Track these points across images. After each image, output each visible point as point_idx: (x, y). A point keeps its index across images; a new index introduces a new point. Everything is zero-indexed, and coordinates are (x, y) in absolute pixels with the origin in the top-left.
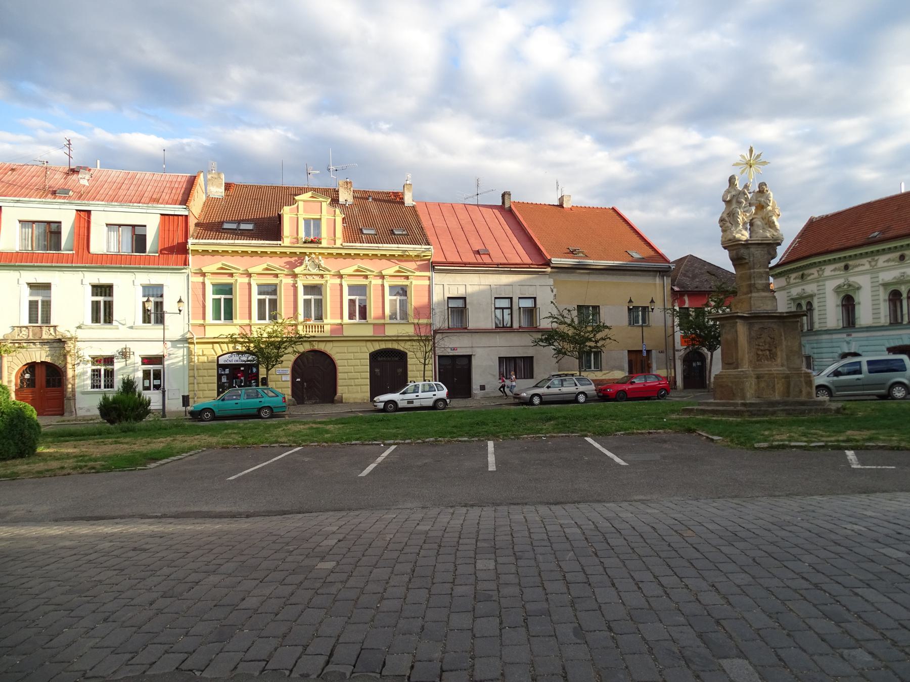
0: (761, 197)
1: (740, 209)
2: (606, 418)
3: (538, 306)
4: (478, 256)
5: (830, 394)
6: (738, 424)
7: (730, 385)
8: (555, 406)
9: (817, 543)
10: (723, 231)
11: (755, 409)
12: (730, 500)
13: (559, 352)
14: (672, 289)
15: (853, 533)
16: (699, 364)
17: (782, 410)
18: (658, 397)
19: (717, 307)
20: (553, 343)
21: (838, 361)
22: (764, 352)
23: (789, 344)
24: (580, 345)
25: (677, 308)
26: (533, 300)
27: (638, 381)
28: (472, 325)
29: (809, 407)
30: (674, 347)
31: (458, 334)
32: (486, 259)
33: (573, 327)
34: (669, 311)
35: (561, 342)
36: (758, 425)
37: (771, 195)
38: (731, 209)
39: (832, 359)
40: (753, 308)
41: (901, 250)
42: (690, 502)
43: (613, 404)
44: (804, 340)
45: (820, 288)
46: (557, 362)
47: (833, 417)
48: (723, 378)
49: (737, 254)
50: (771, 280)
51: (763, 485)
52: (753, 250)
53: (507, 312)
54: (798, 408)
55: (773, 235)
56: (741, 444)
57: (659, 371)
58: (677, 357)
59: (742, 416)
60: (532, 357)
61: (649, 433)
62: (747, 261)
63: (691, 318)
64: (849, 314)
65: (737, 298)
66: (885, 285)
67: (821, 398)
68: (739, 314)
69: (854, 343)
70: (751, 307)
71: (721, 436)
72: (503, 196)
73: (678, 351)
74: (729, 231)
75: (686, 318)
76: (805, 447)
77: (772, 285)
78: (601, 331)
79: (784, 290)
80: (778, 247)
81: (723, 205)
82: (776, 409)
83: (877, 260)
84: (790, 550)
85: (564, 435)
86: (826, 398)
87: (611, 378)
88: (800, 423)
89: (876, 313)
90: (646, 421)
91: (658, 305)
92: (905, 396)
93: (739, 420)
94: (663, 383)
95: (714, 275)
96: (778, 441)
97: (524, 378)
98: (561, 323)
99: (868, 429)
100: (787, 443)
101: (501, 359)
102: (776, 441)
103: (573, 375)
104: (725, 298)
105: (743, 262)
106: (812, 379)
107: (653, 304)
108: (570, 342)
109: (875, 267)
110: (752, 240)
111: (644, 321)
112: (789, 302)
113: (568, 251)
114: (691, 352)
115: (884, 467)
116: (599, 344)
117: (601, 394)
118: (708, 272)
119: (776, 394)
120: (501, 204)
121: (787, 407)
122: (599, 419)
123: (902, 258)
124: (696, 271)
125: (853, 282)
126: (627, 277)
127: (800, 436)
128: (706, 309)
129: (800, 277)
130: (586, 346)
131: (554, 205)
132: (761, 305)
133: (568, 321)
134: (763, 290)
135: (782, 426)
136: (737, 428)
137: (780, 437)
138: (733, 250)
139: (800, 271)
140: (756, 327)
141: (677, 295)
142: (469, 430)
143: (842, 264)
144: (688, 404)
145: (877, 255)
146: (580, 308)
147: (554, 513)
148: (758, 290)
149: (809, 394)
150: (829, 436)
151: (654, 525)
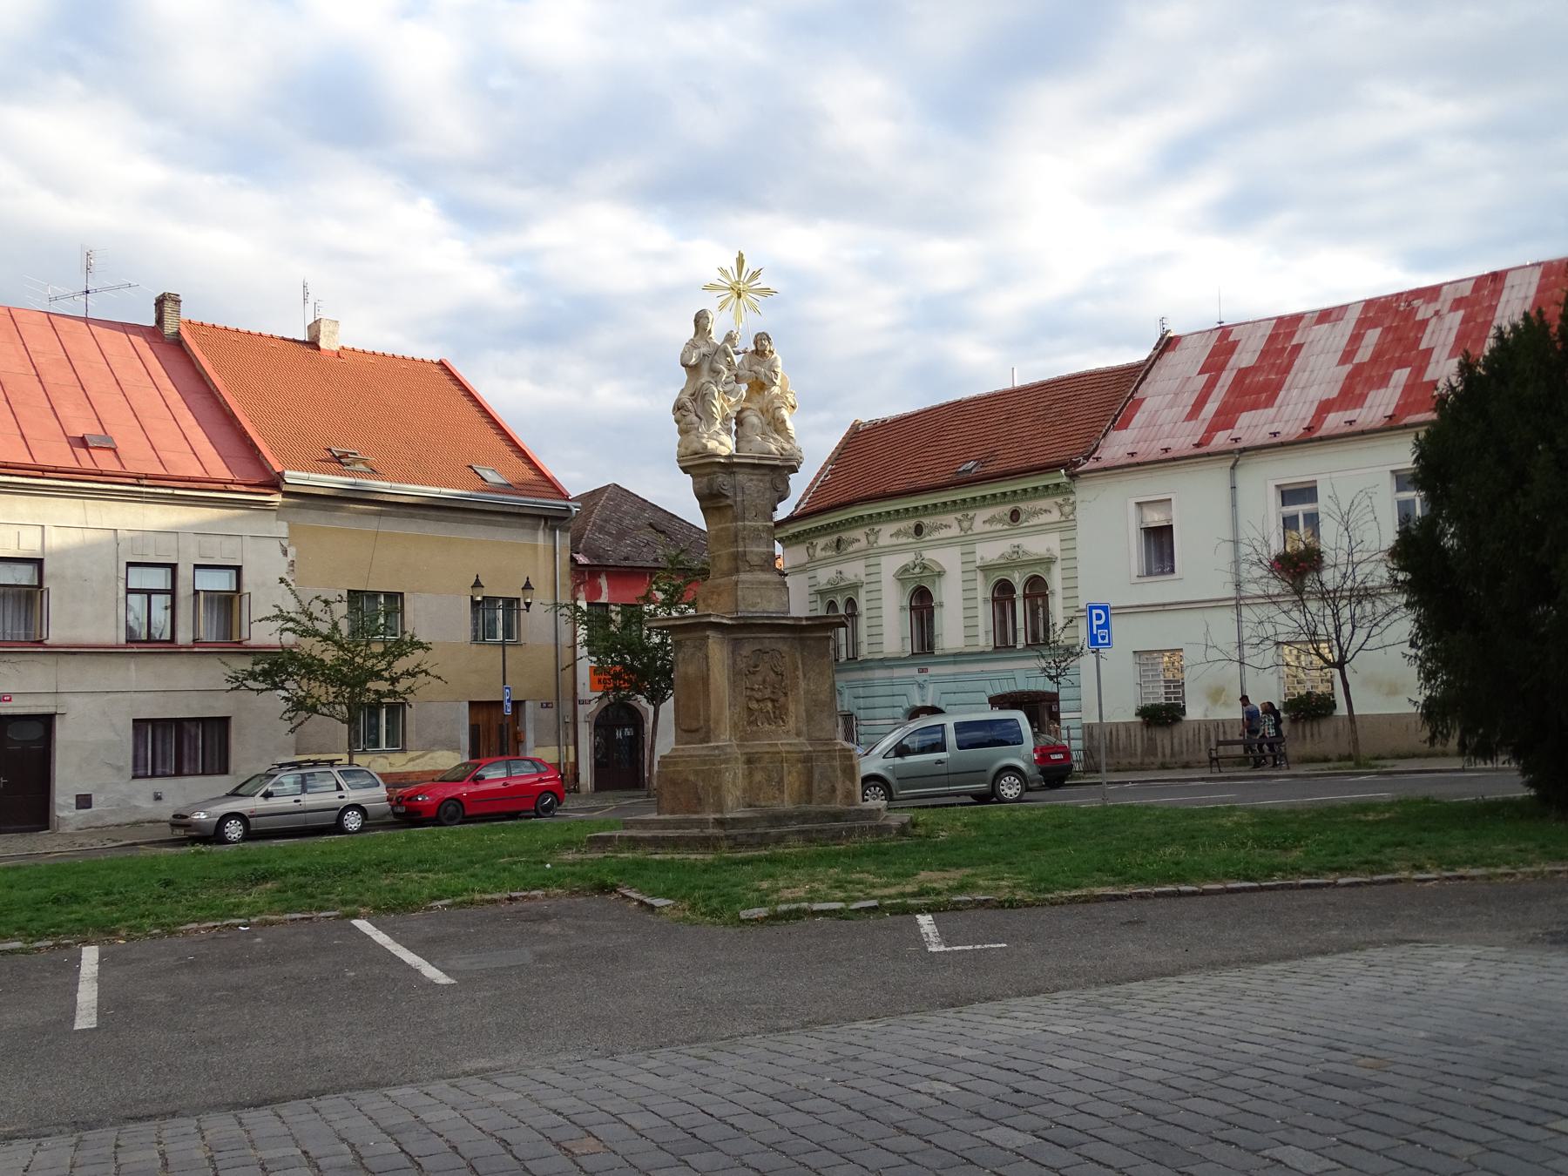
2: (408, 867)
3: (245, 590)
4: (81, 452)
5: (889, 796)
6: (707, 868)
7: (692, 778)
8: (282, 842)
9: (861, 1135)
10: (682, 432)
11: (741, 831)
12: (684, 1048)
13: (299, 705)
14: (573, 560)
15: (933, 1101)
16: (628, 732)
17: (799, 832)
18: (536, 811)
19: (669, 604)
20: (283, 682)
21: (902, 725)
24: (353, 687)
25: (583, 604)
26: (234, 572)
27: (495, 775)
28: (57, 634)
29: (849, 824)
30: (575, 693)
31: (14, 658)
32: (106, 462)
33: (335, 642)
34: (565, 611)
35: (305, 680)
37: (780, 362)
38: (699, 384)
39: (891, 721)
40: (742, 607)
41: (1014, 501)
42: (594, 1063)
43: (429, 833)
44: (841, 680)
45: (872, 570)
46: (292, 731)
48: (676, 764)
49: (710, 486)
50: (778, 549)
51: (755, 1007)
52: (742, 477)
53: (160, 602)
54: (827, 826)
55: (783, 448)
56: (712, 913)
57: (541, 750)
58: (581, 717)
59: (715, 848)
60: (225, 721)
61: (511, 899)
63: (613, 628)
64: (922, 627)
66: (986, 569)
68: (712, 619)
69: (931, 688)
70: (737, 605)
71: (670, 898)
72: (160, 303)
73: (583, 702)
74: (693, 432)
75: (601, 627)
76: (840, 911)
77: (780, 561)
78: (406, 654)
79: (804, 571)
83: (973, 518)
84: (808, 1159)
85: (299, 916)
86: (881, 803)
87: (427, 768)
88: (832, 859)
89: (970, 627)
90: (504, 870)
91: (541, 598)
92: (1021, 795)
93: (709, 857)
94: (549, 779)
95: (663, 532)
96: (787, 901)
97: (203, 774)
98: (306, 633)
99: (958, 866)
100: (805, 905)
101: (139, 724)
102: (782, 902)
103: (331, 763)
104: (686, 584)
105: (721, 505)
106: (855, 762)
107: (528, 592)
108: (329, 680)
109: (969, 532)
111: (508, 632)
113: (329, 455)
114: (611, 704)
115: (986, 946)
116: (400, 687)
117: (401, 809)
118: (651, 525)
119: (786, 796)
120: (153, 323)
121: (807, 826)
122: (390, 870)
125: (930, 560)
126: (470, 527)
127: (831, 888)
128: (646, 608)
129: (834, 545)
130: (368, 690)
131: (295, 341)
132: (758, 602)
133: (324, 628)
134: (762, 568)
135: (797, 868)
136: (706, 876)
137: (792, 891)
140: (747, 650)
141: (583, 573)
142: (30, 920)
143: (1006, 509)
144: (602, 827)
146: (354, 596)
147: (248, 1132)
148: (752, 568)
149: (849, 795)
150: (886, 886)
151: (507, 1136)
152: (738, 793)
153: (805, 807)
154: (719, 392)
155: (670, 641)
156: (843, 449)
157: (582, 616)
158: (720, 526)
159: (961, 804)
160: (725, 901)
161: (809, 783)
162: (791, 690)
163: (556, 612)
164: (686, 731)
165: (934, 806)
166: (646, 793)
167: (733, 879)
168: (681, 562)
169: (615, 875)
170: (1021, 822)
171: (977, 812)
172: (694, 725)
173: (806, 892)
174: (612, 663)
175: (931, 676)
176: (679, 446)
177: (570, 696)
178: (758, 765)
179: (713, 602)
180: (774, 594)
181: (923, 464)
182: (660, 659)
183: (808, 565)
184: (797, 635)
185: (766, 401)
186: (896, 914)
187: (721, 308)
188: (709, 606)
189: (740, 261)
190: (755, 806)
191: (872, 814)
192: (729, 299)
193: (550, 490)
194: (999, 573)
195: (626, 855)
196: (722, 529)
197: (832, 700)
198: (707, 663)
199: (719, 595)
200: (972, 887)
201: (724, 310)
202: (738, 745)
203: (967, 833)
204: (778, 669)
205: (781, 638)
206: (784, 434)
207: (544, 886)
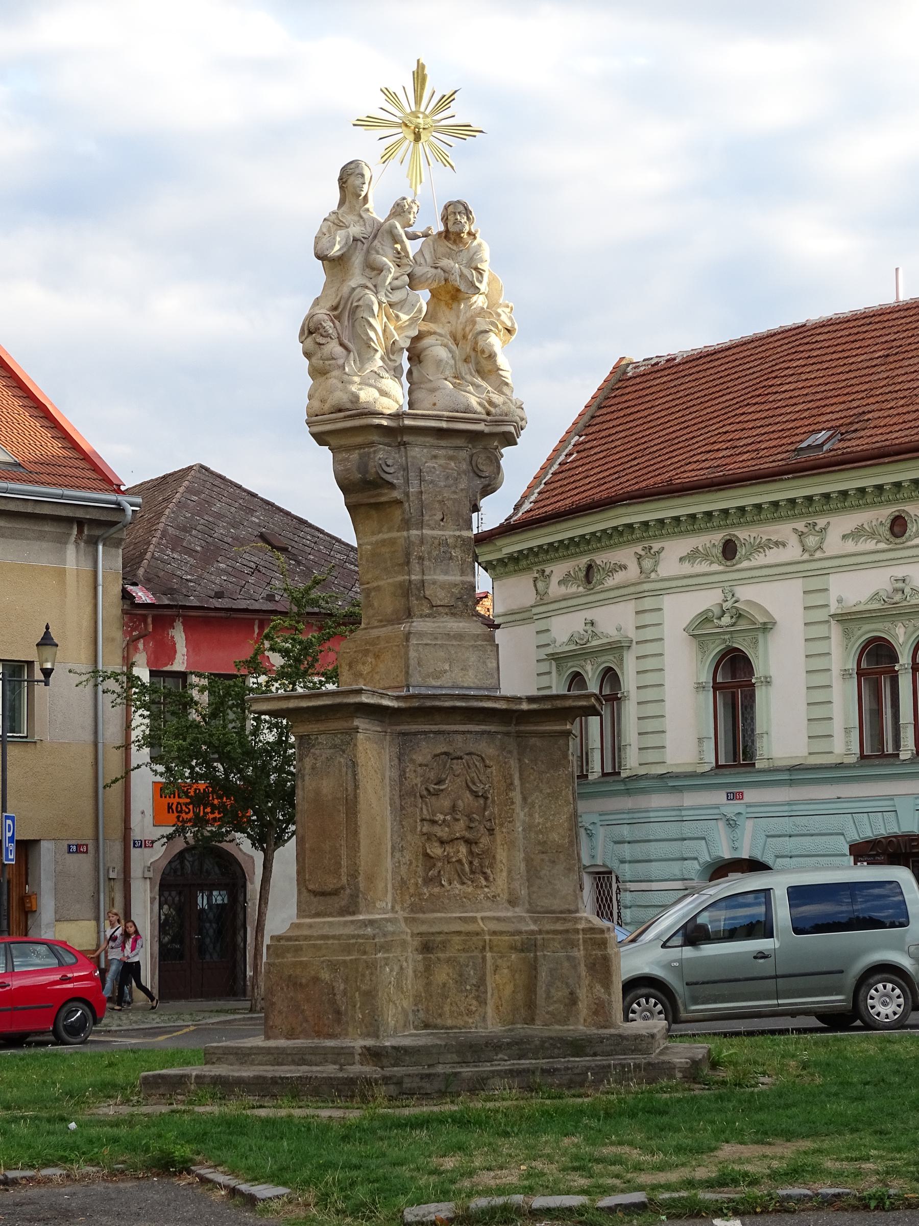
0: (449, 256)
1: (376, 290)
5: (673, 1014)
7: (325, 975)
10: (317, 372)
11: (412, 1070)
14: (126, 596)
16: (219, 897)
17: (511, 1073)
18: (55, 1032)
19: (291, 674)
22: (450, 849)
23: (538, 819)
25: (143, 673)
29: (599, 1060)
34: (111, 684)
36: (422, 1135)
37: (486, 253)
38: (345, 290)
39: (678, 885)
40: (416, 679)
47: (679, 1095)
48: (298, 950)
49: (363, 467)
50: (483, 581)
54: (560, 1063)
55: (491, 403)
58: (136, 870)
59: (364, 1099)
62: (396, 494)
63: (194, 716)
65: (359, 634)
67: (638, 1026)
68: (365, 699)
69: (749, 826)
71: (284, 1184)
73: (141, 844)
74: (335, 373)
75: (173, 713)
79: (529, 620)
80: (507, 451)
81: (318, 273)
82: (487, 1068)
83: (825, 529)
86: (659, 1024)
92: (904, 1015)
93: (354, 1115)
95: (284, 550)
96: (488, 1192)
99: (789, 1135)
100: (518, 1199)
102: (479, 1194)
104: (322, 640)
105: (383, 499)
106: (611, 951)
107: (48, 650)
109: (818, 555)
110: (415, 417)
112: (544, 667)
114: (189, 849)
118: (262, 537)
119: (490, 1010)
121: (525, 1063)
123: (898, 526)
124: (220, 531)
125: (749, 602)
127: (564, 1169)
128: (251, 681)
129: (582, 575)
134: (452, 611)
135: (506, 1134)
136: (347, 1147)
138: (349, 449)
139: (582, 553)
140: (424, 753)
141: (144, 618)
144: (169, 1062)
145: (822, 512)
148: (435, 610)
149: (600, 1009)
150: (660, 1168)
152: (405, 1004)
153: (522, 1029)
154: (380, 303)
155: (292, 739)
156: (600, 408)
157: (142, 693)
158: (381, 536)
159: (800, 1031)
160: (380, 1191)
161: (531, 988)
162: (502, 825)
163: (96, 685)
164: (315, 893)
165: (750, 1034)
166: (247, 1004)
167: (394, 1153)
168: (314, 602)
169: (188, 1142)
170: (901, 1062)
171: (826, 1044)
172: (331, 883)
173: (521, 1177)
174: (191, 776)
175: (749, 805)
176: (310, 397)
177: (118, 834)
178: (441, 955)
179: (365, 669)
180: (473, 658)
181: (737, 435)
182: (276, 769)
183: (535, 610)
184: (512, 729)
185: (462, 319)
186: (678, 1217)
187: (386, 158)
188: (358, 675)
189: (420, 77)
190: (436, 1027)
191: (640, 1043)
192: (398, 143)
193: (82, 464)
194: (873, 626)
195: (208, 1109)
196: (383, 542)
197: (571, 843)
198: (355, 774)
199: (377, 656)
200: (813, 1173)
201: (391, 162)
202: (406, 919)
203: (807, 1079)
204: (479, 788)
205: (483, 733)
206: (493, 378)
207: (65, 1159)
